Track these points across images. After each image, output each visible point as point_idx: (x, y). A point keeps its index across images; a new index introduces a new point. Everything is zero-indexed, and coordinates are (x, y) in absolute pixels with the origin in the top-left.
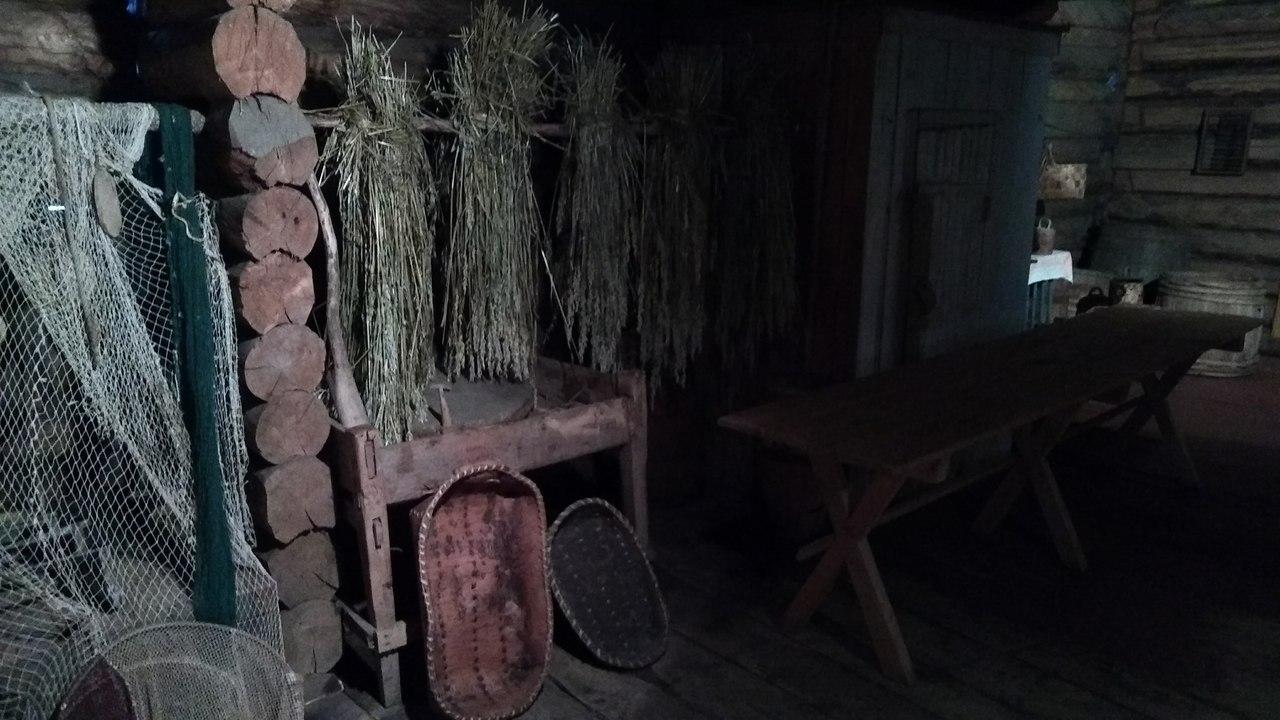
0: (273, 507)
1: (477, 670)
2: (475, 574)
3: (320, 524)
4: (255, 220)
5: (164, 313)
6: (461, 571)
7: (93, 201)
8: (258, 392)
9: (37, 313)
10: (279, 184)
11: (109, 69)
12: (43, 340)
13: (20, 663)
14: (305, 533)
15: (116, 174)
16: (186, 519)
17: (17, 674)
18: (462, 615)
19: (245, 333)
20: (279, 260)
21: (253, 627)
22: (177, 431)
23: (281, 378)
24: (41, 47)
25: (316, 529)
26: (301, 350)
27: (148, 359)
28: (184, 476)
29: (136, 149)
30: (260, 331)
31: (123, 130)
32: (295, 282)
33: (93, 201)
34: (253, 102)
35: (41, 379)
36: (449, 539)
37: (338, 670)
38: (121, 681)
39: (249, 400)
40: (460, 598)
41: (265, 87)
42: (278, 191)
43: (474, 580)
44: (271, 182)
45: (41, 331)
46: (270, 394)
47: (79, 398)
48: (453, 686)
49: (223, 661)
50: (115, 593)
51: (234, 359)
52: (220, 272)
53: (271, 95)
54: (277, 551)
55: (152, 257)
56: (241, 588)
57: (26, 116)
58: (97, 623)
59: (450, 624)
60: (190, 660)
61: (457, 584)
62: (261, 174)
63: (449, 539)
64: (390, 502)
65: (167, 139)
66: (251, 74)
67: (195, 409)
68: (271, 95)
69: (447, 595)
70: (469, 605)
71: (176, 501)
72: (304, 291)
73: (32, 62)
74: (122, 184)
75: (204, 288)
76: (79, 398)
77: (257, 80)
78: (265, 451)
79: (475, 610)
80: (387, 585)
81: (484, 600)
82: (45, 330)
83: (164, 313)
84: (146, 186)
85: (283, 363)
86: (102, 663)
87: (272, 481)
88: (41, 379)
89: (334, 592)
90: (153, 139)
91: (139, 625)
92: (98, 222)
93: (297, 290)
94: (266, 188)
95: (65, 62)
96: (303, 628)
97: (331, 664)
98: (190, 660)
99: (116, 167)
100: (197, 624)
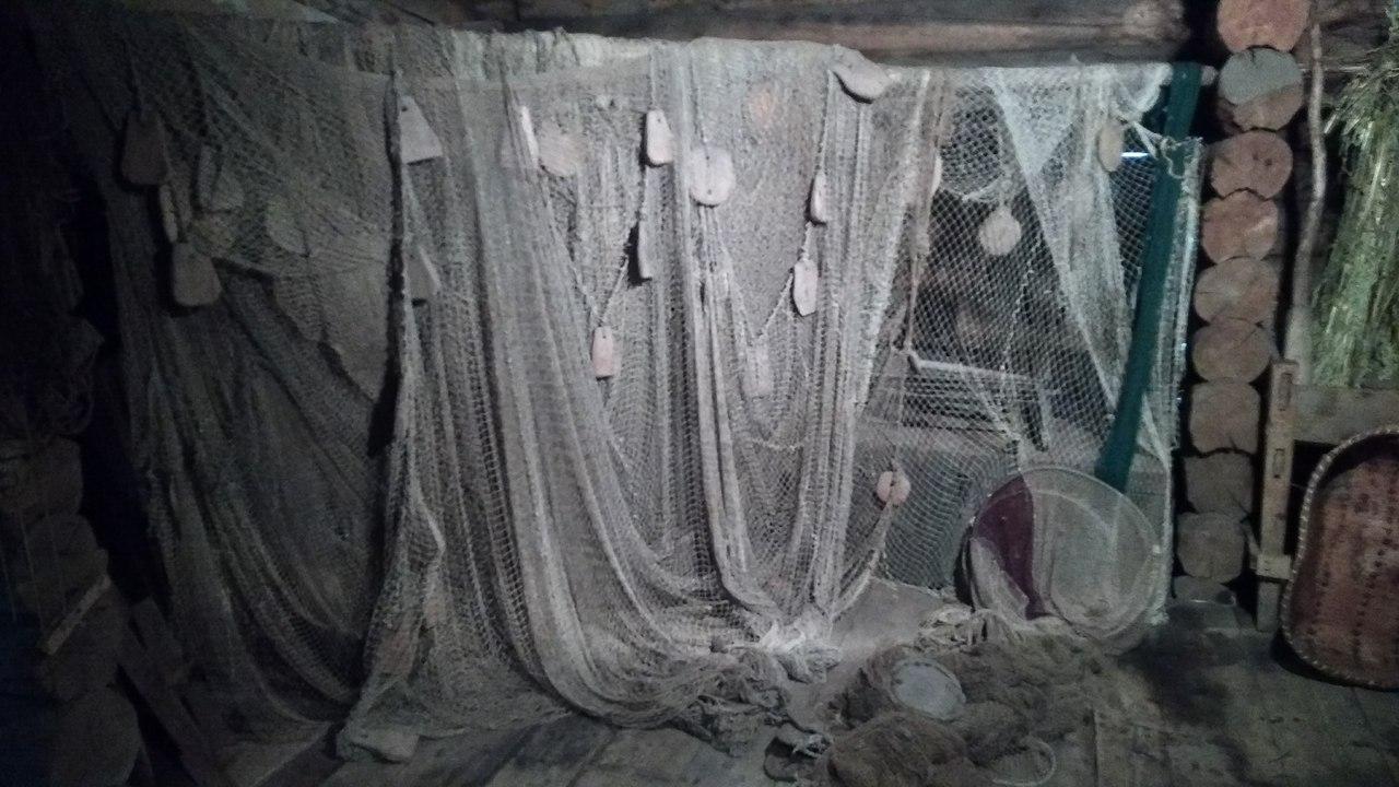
0: (1197, 418)
1: (1356, 633)
2: (1387, 542)
3: (1240, 447)
4: (1227, 162)
5: (1137, 236)
6: (1367, 533)
7: (1097, 143)
8: (1203, 313)
9: (1038, 223)
10: (1255, 129)
11: (1187, 34)
12: (1038, 244)
13: (974, 457)
14: (1225, 450)
15: (1124, 122)
16: (1112, 399)
17: (970, 463)
18: (1355, 575)
19: (1203, 262)
20: (1246, 198)
21: (1141, 500)
22: (1123, 333)
23: (1227, 305)
24: (1135, 23)
25: (1237, 451)
26: (1252, 283)
27: (1114, 272)
28: (1120, 368)
29: (1146, 101)
30: (1215, 260)
31: (1137, 87)
32: (1258, 220)
33: (1097, 143)
34: (1248, 54)
35: (1031, 271)
36: (1365, 498)
37: (1231, 585)
38: (1030, 497)
39: (1195, 323)
40: (1360, 559)
41: (1261, 41)
42: (1252, 136)
43: (1384, 547)
44: (1247, 126)
45: (1038, 237)
46: (1213, 318)
47: (1053, 289)
48: (1320, 634)
49: (1108, 515)
50: (1047, 437)
51: (1188, 281)
52: (1190, 207)
53: (1267, 47)
54: (1195, 458)
55: (1141, 190)
56: (1138, 464)
57: (1063, 80)
58: (1025, 450)
59: (1336, 576)
60: (1082, 504)
61: (1360, 544)
62: (1238, 119)
63: (1365, 498)
64: (1307, 438)
65: (1175, 91)
66: (1250, 30)
67: (1142, 321)
68: (1267, 47)
69: (1345, 547)
70: (1369, 568)
71: (1110, 385)
72: (1267, 229)
73: (1126, 36)
74: (1129, 130)
75: (1171, 218)
76: (1053, 289)
77: (1255, 35)
78: (1200, 367)
79: (1373, 576)
80: (1279, 516)
81: (1389, 571)
82: (1042, 236)
83: (1137, 236)
84: (1148, 132)
85: (1233, 293)
86: (1019, 479)
87: (1200, 394)
88: (1031, 271)
89: (1245, 515)
90: (1166, 90)
91: (1052, 463)
92: (1099, 160)
93: (1260, 227)
94: (1243, 132)
95: (1150, 33)
96: (1207, 533)
97: (1228, 578)
98: (1082, 504)
99: (1125, 116)
100: (1093, 478)
